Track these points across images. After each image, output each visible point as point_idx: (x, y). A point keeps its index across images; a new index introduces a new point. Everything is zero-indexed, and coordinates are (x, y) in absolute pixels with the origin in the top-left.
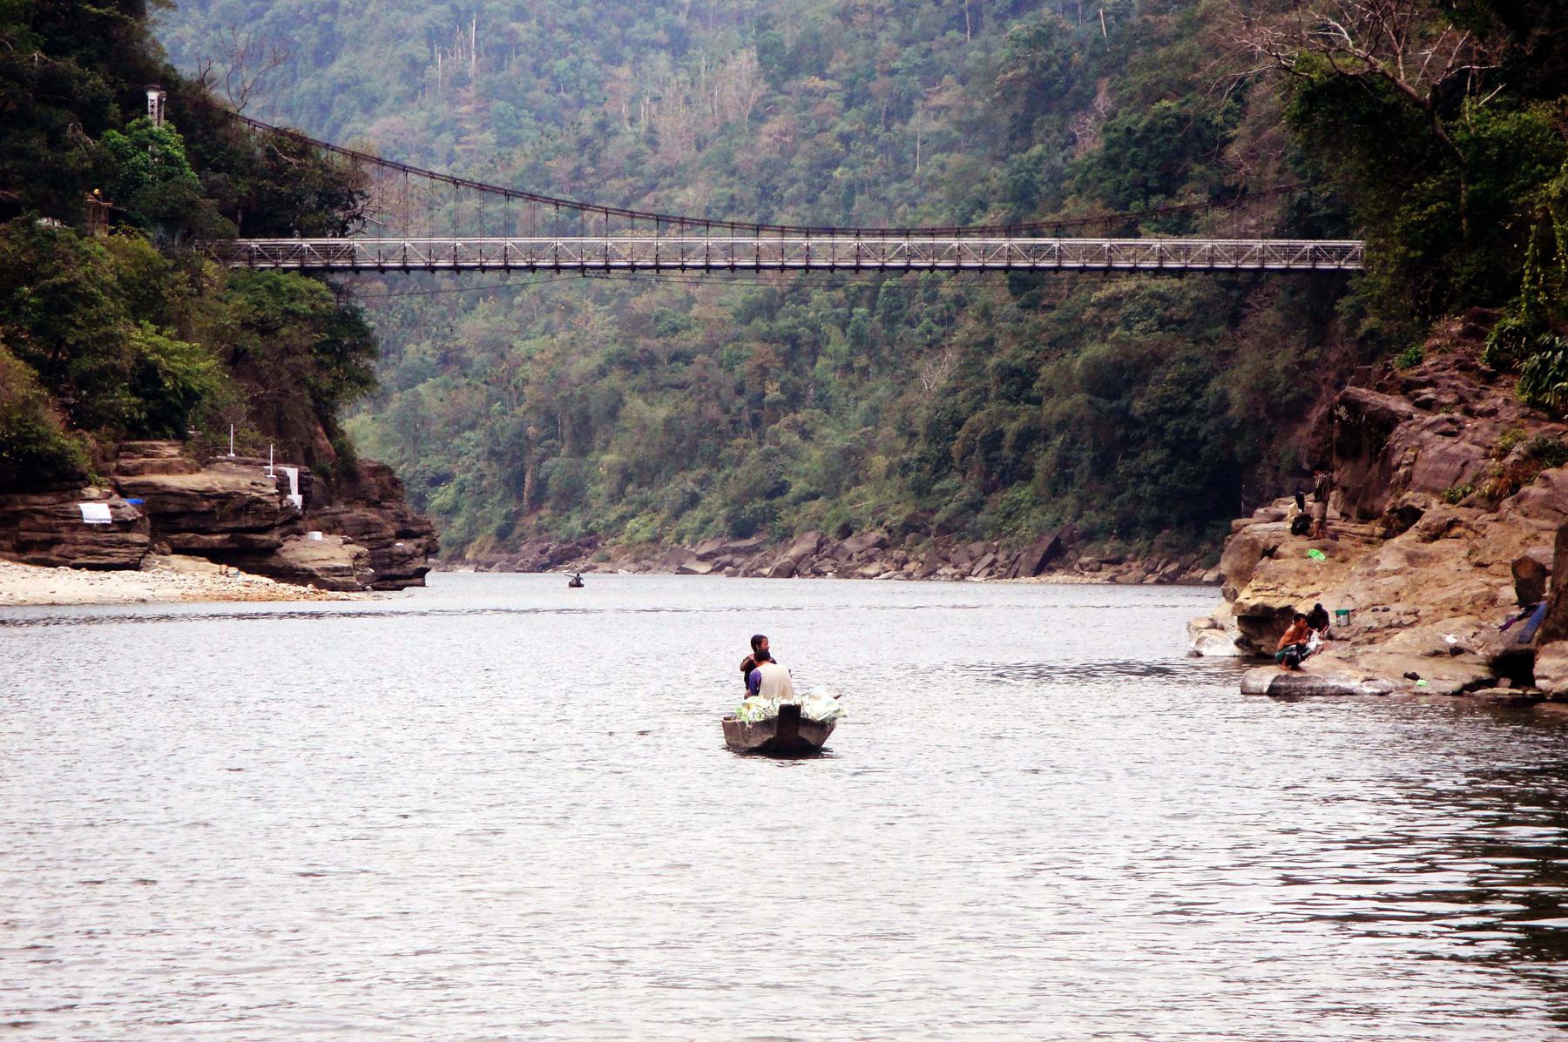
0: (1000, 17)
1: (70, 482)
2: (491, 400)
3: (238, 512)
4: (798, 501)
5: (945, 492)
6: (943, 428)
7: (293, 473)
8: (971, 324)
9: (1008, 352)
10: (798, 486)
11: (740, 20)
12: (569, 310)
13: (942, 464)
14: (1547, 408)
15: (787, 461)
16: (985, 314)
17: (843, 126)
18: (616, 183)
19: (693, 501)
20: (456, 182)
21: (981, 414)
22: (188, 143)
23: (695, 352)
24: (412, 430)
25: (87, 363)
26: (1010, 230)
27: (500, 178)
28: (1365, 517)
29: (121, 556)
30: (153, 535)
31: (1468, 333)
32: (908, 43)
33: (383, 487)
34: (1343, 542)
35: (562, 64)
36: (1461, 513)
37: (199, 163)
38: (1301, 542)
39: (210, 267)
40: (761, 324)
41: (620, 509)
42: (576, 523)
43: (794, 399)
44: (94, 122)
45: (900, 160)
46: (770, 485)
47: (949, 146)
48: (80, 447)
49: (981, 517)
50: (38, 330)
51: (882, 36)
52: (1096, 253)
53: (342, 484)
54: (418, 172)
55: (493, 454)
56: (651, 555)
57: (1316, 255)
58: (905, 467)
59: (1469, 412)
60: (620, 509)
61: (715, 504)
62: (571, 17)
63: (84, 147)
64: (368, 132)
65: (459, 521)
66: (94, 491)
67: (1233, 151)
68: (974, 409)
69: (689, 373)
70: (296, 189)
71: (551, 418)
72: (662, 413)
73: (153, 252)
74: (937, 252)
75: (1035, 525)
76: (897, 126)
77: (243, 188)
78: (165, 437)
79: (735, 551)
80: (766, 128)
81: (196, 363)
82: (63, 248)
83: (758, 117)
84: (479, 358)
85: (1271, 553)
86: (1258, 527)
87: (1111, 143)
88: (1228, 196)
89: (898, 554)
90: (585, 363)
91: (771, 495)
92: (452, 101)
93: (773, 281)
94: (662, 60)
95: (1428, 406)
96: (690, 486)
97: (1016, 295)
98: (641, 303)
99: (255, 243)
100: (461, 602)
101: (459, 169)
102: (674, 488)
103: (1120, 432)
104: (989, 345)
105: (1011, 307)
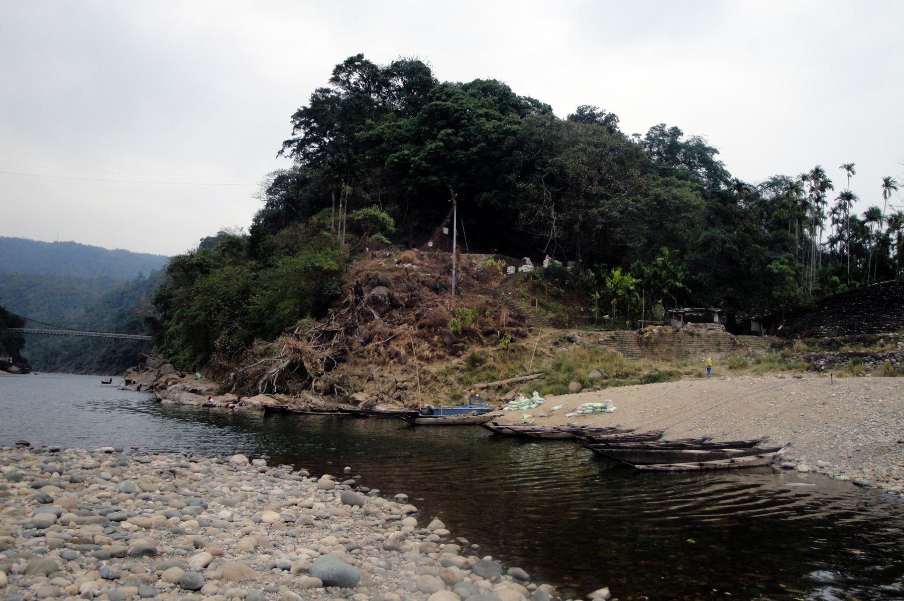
6: (104, 357)
33: (24, 361)
43: (85, 352)
56: (65, 371)
64: (31, 316)
86: (129, 370)
88: (142, 331)
98: (66, 339)
100: (31, 378)
102: (68, 363)
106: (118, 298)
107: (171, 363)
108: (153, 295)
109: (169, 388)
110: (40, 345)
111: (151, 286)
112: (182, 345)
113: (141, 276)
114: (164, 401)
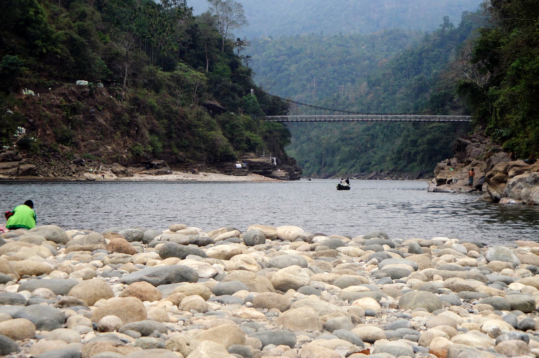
0: (414, 76)
1: (234, 160)
2: (316, 147)
3: (264, 166)
4: (373, 166)
5: (400, 164)
6: (400, 152)
7: (275, 159)
8: (405, 132)
9: (412, 137)
10: (373, 163)
11: (364, 76)
12: (331, 130)
13: (400, 159)
14: (496, 142)
15: (371, 158)
16: (408, 130)
17: (384, 96)
18: (341, 107)
19: (354, 166)
20: (311, 106)
21: (407, 149)
22: (258, 99)
23: (355, 137)
24: (301, 153)
25: (238, 138)
26: (415, 114)
27: (319, 106)
28: (462, 162)
29: (243, 173)
30: (249, 170)
31: (483, 128)
32: (396, 80)
33: (294, 161)
34: (457, 167)
35: (331, 85)
36: (479, 162)
37: (260, 102)
38: (449, 167)
39: (261, 121)
40: (367, 133)
41: (340, 167)
42: (332, 170)
43: (373, 146)
44: (240, 95)
45: (394, 102)
46: (368, 163)
47: (403, 99)
48: (236, 154)
49: (407, 168)
50: (229, 132)
51: (391, 79)
52: (427, 118)
53: (285, 161)
54: (304, 104)
55: (317, 157)
57: (469, 119)
58: (392, 159)
59: (482, 143)
60: (340, 167)
61: (358, 166)
62: (333, 76)
63: (238, 99)
65: (310, 169)
66: (238, 162)
67: (455, 100)
68: (406, 148)
69: (353, 142)
70: (277, 106)
71: (327, 150)
72: (348, 149)
73: (250, 118)
74: (397, 118)
75: (417, 170)
76: (393, 96)
77: (268, 107)
78: (251, 152)
79: (361, 175)
80: (369, 96)
81: (257, 138)
82: (234, 117)
83: (367, 94)
84: (314, 139)
85: (443, 169)
86: (441, 164)
87: (432, 98)
88: (455, 108)
89: (391, 175)
90: (333, 140)
91: (368, 165)
92: (311, 92)
93: (370, 125)
94: (349, 84)
95: (474, 142)
96: (353, 163)
97: (414, 126)
98: (344, 129)
99: (270, 117)
101: (312, 104)
103: (433, 152)
104: (408, 136)
105: (413, 129)
106: (415, 62)
107: (506, 150)
108: (469, 49)
109: (511, 181)
110: (309, 139)
111: (463, 38)
112: (523, 121)
113: (447, 23)
114: (504, 201)
